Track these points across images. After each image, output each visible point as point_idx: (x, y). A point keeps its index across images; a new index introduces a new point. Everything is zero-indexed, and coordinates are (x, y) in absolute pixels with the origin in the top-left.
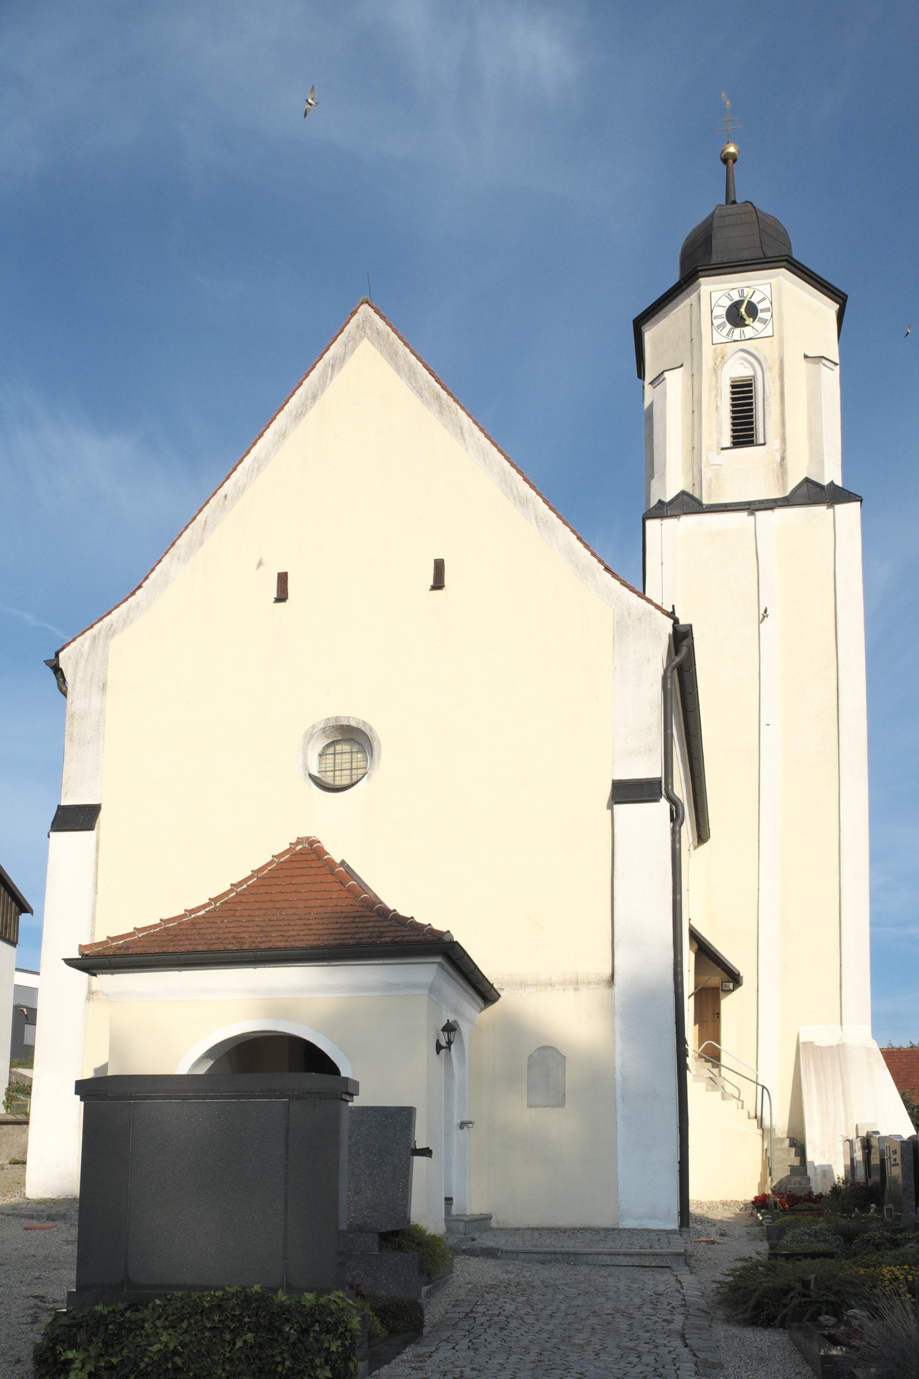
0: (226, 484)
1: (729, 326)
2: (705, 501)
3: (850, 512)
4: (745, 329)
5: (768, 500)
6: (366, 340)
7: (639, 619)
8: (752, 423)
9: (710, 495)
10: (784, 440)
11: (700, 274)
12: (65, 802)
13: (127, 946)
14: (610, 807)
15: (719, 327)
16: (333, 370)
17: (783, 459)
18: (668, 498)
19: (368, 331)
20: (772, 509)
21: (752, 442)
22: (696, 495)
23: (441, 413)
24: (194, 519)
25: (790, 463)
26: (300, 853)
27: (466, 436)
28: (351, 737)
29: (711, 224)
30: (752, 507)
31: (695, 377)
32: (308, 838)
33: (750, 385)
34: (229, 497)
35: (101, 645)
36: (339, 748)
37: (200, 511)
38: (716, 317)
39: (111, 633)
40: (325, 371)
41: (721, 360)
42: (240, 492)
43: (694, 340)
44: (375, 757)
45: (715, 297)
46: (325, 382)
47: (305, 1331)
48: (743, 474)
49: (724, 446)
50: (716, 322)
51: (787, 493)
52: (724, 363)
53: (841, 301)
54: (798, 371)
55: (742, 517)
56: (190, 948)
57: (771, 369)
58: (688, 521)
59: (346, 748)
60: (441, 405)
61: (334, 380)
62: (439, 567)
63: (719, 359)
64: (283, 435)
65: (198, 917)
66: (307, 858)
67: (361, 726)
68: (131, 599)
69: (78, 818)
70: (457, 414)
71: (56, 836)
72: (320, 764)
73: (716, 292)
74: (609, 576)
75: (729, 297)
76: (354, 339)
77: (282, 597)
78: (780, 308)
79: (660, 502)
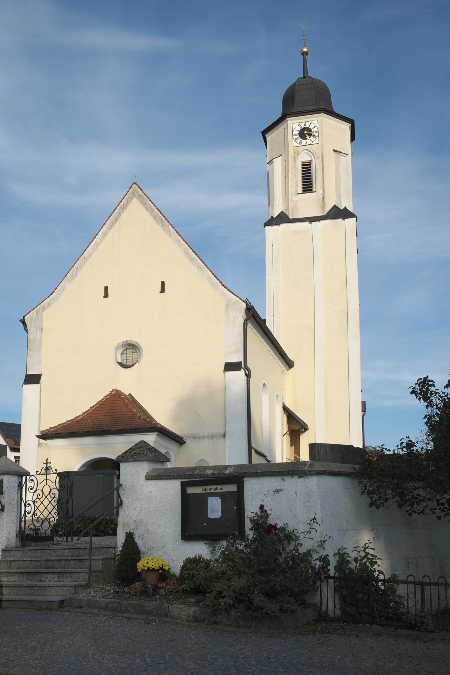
0: (85, 253)
1: (300, 139)
2: (291, 217)
3: (351, 221)
4: (307, 140)
5: (317, 217)
6: (135, 200)
7: (234, 303)
8: (311, 181)
9: (293, 215)
10: (324, 190)
11: (287, 116)
12: (29, 373)
13: (56, 431)
14: (224, 372)
15: (296, 139)
16: (123, 209)
17: (323, 198)
18: (275, 216)
19: (136, 195)
20: (319, 221)
21: (311, 190)
22: (287, 214)
23: (163, 226)
24: (73, 266)
25: (327, 200)
26: (113, 395)
27: (172, 235)
28: (131, 347)
29: (294, 89)
30: (311, 220)
31: (286, 161)
32: (116, 389)
33: (310, 164)
34: (86, 258)
35: (40, 313)
36: (128, 351)
37: (76, 263)
38: (295, 135)
39: (44, 309)
40: (120, 210)
41: (297, 154)
42: (90, 256)
43: (286, 144)
44: (141, 353)
45: (294, 126)
46: (120, 214)
47: (107, 523)
48: (307, 205)
49: (299, 193)
50: (295, 137)
51: (325, 214)
52: (298, 156)
53: (351, 123)
54: (331, 157)
55: (306, 224)
56: (77, 431)
57: (318, 158)
58: (283, 226)
59: (131, 351)
60: (162, 223)
61: (124, 213)
62: (163, 284)
63: (296, 154)
64: (105, 234)
65: (79, 419)
66: (116, 397)
67: (136, 344)
68: (51, 297)
69: (33, 379)
70: (168, 227)
71: (26, 386)
72: (121, 357)
73: (294, 124)
74: (223, 287)
75: (300, 126)
76: (131, 198)
77: (106, 295)
78: (322, 131)
79: (272, 217)
